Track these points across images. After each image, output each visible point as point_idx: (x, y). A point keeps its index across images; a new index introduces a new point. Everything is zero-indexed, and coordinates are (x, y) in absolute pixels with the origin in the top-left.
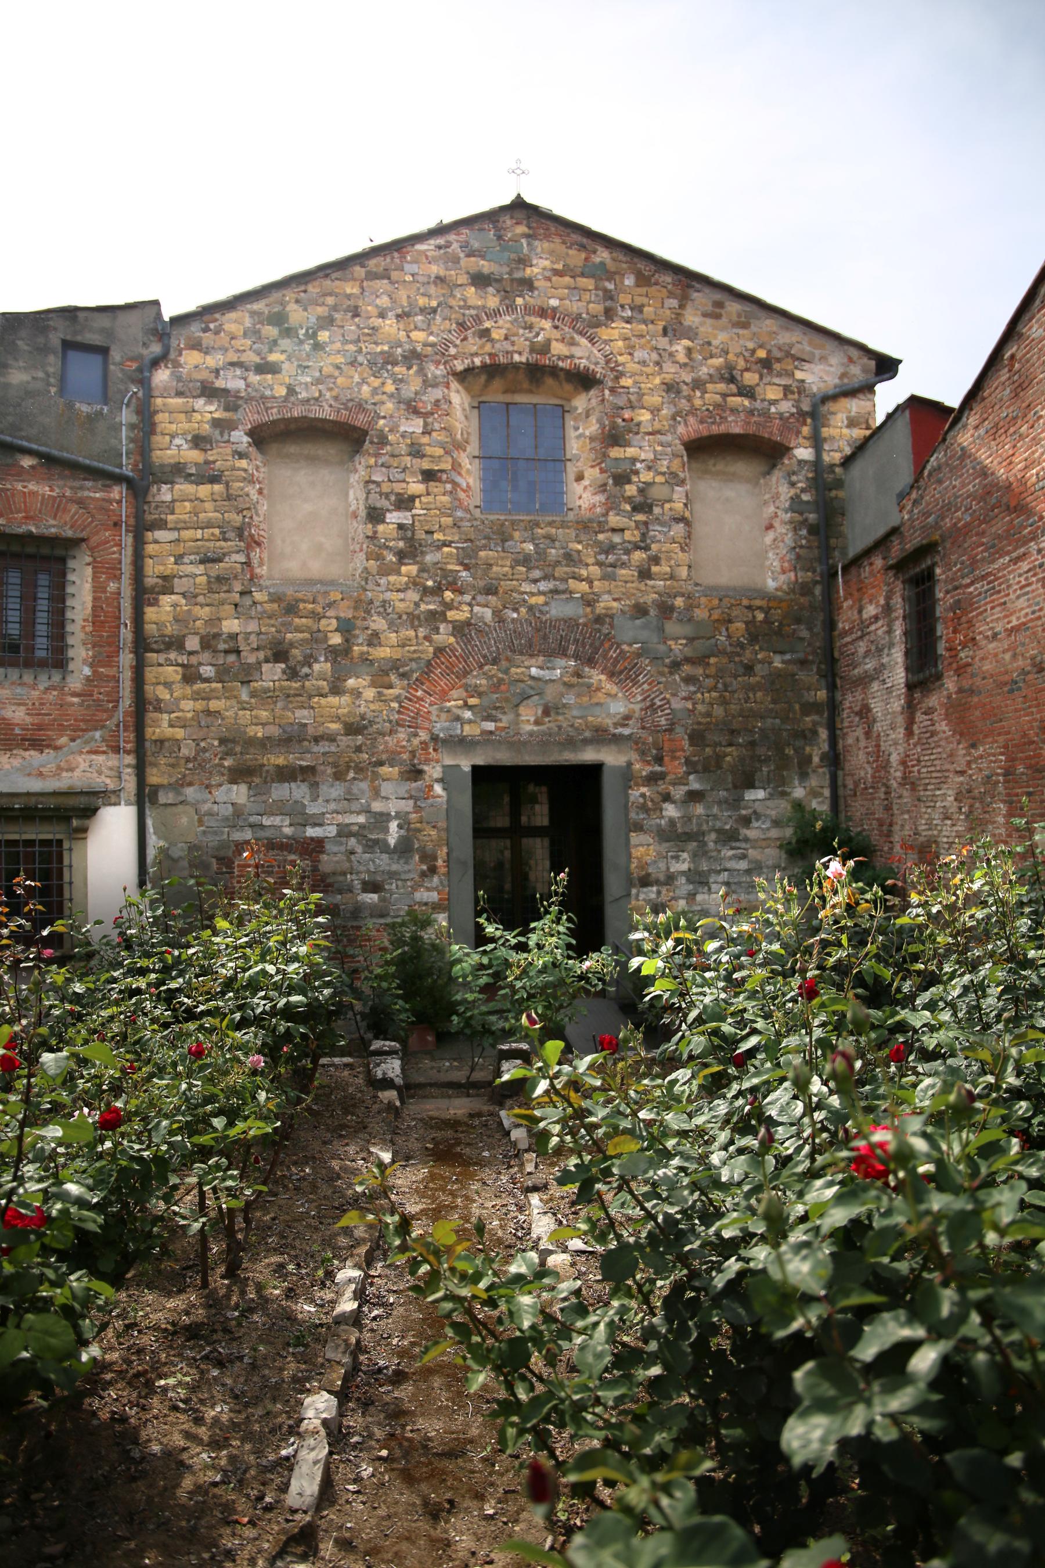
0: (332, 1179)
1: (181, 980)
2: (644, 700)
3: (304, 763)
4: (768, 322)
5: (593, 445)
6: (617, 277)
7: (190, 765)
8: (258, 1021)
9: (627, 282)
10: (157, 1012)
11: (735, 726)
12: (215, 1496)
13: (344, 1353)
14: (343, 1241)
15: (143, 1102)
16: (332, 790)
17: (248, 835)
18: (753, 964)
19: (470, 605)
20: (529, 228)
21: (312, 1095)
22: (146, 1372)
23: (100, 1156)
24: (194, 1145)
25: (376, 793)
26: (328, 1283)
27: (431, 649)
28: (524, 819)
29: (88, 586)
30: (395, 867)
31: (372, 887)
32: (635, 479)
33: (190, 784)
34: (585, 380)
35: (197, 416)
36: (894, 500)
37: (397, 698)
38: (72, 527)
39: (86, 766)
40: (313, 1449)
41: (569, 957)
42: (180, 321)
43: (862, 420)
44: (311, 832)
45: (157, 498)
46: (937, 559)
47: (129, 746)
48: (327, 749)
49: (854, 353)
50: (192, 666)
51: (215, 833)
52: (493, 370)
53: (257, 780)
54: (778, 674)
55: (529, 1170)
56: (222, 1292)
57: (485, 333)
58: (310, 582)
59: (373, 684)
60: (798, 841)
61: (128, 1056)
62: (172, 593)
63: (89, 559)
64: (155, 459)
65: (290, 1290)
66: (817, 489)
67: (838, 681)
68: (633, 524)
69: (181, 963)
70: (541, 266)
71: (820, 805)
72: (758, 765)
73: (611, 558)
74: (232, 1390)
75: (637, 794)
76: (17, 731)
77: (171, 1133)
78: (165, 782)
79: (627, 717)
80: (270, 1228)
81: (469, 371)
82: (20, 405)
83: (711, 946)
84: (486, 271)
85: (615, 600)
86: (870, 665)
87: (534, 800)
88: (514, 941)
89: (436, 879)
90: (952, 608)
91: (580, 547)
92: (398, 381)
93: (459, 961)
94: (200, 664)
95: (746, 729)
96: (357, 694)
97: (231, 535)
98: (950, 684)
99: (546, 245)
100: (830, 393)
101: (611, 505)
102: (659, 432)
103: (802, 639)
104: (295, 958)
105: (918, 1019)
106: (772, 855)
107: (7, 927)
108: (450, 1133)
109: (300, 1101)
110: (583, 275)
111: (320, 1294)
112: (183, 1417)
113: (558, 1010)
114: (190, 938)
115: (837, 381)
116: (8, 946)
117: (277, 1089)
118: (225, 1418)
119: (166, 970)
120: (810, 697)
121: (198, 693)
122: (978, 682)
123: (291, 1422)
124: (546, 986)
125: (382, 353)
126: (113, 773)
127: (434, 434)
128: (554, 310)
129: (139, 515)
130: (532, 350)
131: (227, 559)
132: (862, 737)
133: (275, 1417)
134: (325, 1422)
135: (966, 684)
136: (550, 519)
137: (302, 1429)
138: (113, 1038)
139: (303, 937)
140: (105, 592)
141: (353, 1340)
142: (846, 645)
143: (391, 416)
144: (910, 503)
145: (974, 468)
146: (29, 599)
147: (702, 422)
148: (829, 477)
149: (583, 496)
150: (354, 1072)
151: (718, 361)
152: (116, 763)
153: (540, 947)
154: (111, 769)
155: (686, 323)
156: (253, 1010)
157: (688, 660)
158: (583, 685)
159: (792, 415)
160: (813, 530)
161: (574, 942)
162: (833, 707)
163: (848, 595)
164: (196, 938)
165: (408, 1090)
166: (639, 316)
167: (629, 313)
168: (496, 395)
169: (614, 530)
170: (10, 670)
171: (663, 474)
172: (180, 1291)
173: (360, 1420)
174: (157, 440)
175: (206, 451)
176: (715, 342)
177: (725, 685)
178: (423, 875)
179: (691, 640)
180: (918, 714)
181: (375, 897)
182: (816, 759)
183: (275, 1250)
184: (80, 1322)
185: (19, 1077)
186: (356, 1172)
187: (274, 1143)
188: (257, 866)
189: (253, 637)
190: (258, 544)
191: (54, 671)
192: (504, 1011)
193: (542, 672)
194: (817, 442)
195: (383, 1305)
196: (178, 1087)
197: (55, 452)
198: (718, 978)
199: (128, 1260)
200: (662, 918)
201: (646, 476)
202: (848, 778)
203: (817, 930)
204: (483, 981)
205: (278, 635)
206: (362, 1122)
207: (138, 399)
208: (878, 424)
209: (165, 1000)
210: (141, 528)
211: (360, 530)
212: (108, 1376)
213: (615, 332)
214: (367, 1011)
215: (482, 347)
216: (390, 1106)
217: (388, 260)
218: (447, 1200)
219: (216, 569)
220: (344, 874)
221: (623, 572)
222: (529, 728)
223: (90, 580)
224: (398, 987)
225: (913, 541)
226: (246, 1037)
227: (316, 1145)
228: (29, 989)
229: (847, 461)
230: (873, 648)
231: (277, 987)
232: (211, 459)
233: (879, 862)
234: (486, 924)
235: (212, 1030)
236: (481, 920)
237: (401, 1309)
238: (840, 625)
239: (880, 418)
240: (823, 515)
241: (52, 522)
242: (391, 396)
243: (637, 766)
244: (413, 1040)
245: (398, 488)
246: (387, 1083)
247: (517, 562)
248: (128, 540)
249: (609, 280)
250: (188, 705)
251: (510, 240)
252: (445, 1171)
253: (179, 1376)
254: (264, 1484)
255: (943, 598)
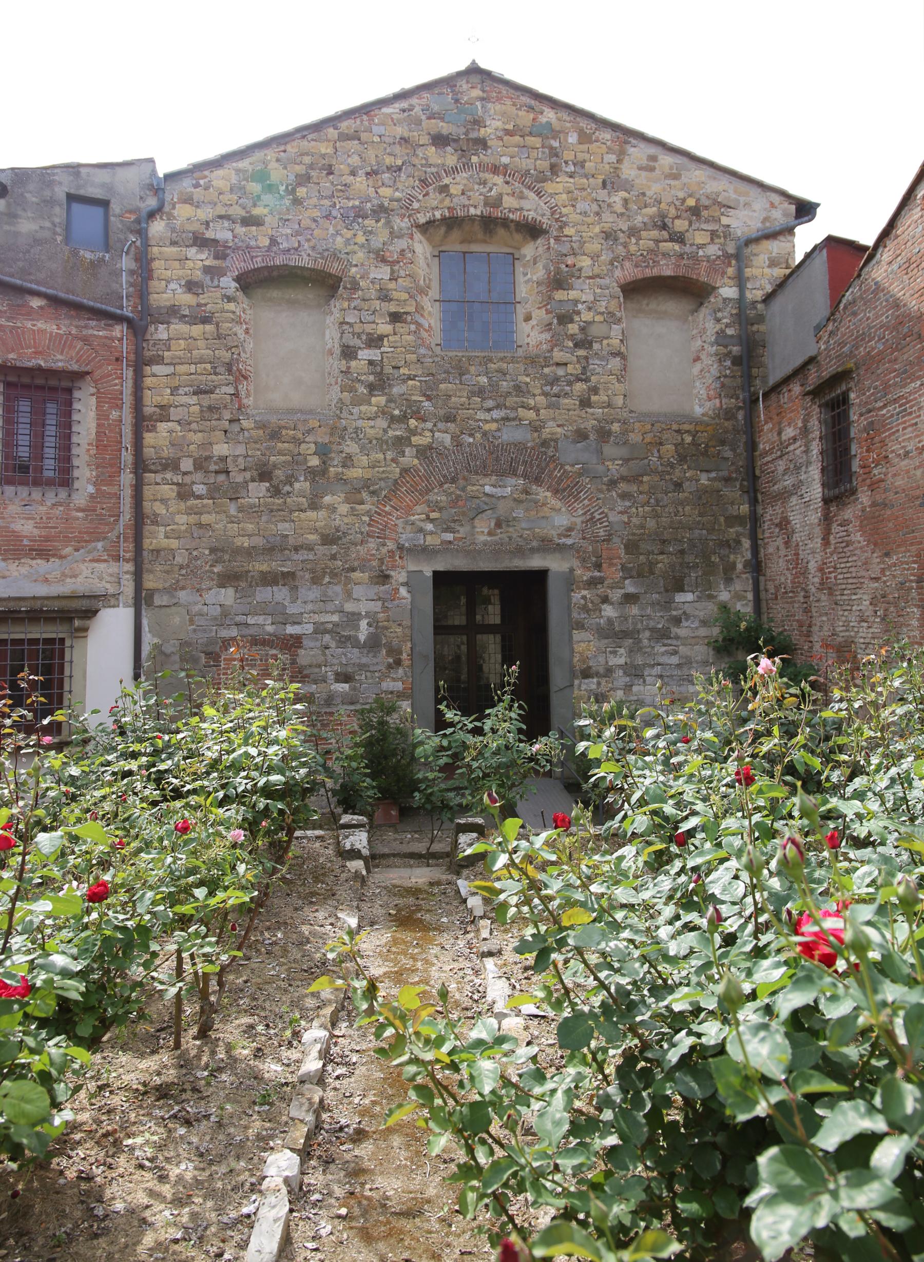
0: (301, 944)
1: (170, 762)
2: (585, 514)
3: (286, 570)
4: (697, 173)
5: (540, 288)
6: (562, 136)
7: (184, 572)
8: (240, 798)
9: (570, 140)
10: (147, 792)
11: (666, 536)
12: (174, 1253)
13: (308, 1111)
14: (310, 1003)
15: (129, 875)
16: (310, 593)
17: (234, 632)
18: (689, 750)
19: (431, 431)
20: (483, 91)
21: (287, 866)
22: (115, 1131)
23: (86, 927)
24: (175, 914)
25: (349, 595)
26: (295, 1043)
27: (398, 470)
28: (478, 617)
29: (92, 414)
30: (364, 660)
31: (345, 677)
32: (577, 318)
33: (183, 588)
34: (533, 231)
35: (190, 264)
36: (812, 333)
37: (368, 513)
38: (77, 361)
39: (87, 573)
40: (274, 1207)
41: (520, 741)
42: (169, 177)
43: (782, 260)
44: (291, 630)
45: (155, 337)
46: (852, 384)
47: (128, 555)
48: (306, 557)
49: (776, 198)
50: (186, 485)
51: (205, 631)
52: (452, 223)
53: (243, 584)
54: (705, 491)
55: (484, 936)
56: (193, 1053)
57: (444, 189)
58: (291, 411)
59: (347, 501)
60: (724, 640)
61: (117, 833)
62: (169, 421)
63: (93, 390)
64: (152, 302)
65: (259, 1049)
66: (740, 324)
67: (760, 497)
68: (575, 359)
69: (170, 747)
70: (494, 126)
71: (745, 608)
72: (686, 571)
73: (556, 389)
74: (197, 1148)
75: (579, 596)
76: (26, 542)
77: (154, 903)
78: (161, 586)
79: (570, 529)
80: (242, 990)
81: (430, 223)
82: (28, 251)
83: (649, 733)
84: (445, 132)
85: (558, 426)
86: (789, 482)
87: (487, 601)
88: (470, 726)
89: (401, 671)
90: (865, 430)
91: (528, 380)
92: (368, 233)
93: (421, 743)
94: (194, 483)
95: (676, 540)
96: (332, 509)
97: (221, 369)
98: (864, 498)
99: (498, 107)
100: (754, 236)
101: (555, 343)
102: (598, 276)
103: (727, 459)
104: (275, 742)
105: (850, 808)
106: (701, 651)
107: (9, 717)
108: (411, 900)
109: (275, 871)
110: (531, 134)
111: (285, 1053)
112: (148, 1175)
113: (510, 788)
114: (180, 724)
115: (760, 225)
116: (10, 735)
117: (255, 859)
118: (188, 1176)
119: (156, 753)
120: (733, 510)
121: (191, 509)
122: (891, 496)
123: (253, 1180)
124: (499, 766)
125: (353, 207)
126: (113, 579)
127: (400, 280)
128: (506, 166)
129: (138, 352)
130: (486, 204)
131: (217, 391)
132: (782, 547)
133: (238, 1175)
134: (287, 1181)
135: (879, 498)
136: (502, 355)
137: (263, 1187)
138: (104, 816)
139: (282, 723)
140: (108, 419)
141: (316, 1099)
142: (766, 464)
143: (362, 265)
144: (827, 334)
145: (887, 301)
146: (38, 424)
147: (636, 266)
148: (752, 313)
149: (531, 334)
150: (325, 844)
151: (652, 211)
152: (116, 570)
153: (494, 731)
154: (111, 575)
155: (623, 177)
156: (235, 788)
157: (623, 478)
158: (531, 501)
159: (719, 257)
160: (737, 361)
161: (524, 727)
162: (755, 520)
163: (769, 419)
164: (186, 724)
165: (373, 860)
166: (581, 171)
167: (572, 169)
168: (454, 245)
169: (558, 364)
170: (20, 488)
171: (602, 314)
172: (153, 1052)
173: (321, 1178)
174: (154, 284)
175: (198, 295)
176: (648, 193)
177: (657, 501)
178: (390, 667)
179: (626, 460)
180: (834, 525)
181: (346, 686)
182: (740, 566)
183: (246, 1011)
184: (55, 1086)
185: (13, 855)
186: (323, 937)
187: (250, 910)
188: (242, 660)
189: (240, 460)
190: (246, 378)
191: (60, 489)
192: (462, 788)
193: (494, 490)
194: (741, 281)
195: (347, 1064)
196: (163, 861)
197: (62, 295)
198: (656, 762)
199: (105, 1024)
200: (606, 707)
201: (587, 316)
202: (769, 583)
203: (745, 721)
204: (442, 762)
205: (263, 458)
206: (331, 890)
207: (136, 247)
208: (797, 262)
209: (155, 780)
210: (140, 364)
211: (335, 366)
212: (77, 1136)
213: (559, 186)
214: (338, 787)
215: (442, 201)
216: (357, 875)
217: (358, 122)
218: (409, 963)
219: (206, 400)
220: (320, 666)
221: (566, 401)
222: (483, 538)
223: (94, 408)
224: (367, 767)
225: (829, 369)
226: (228, 813)
227: (288, 912)
228: (28, 774)
229: (768, 298)
230: (792, 466)
231: (257, 768)
232: (203, 302)
233: (800, 660)
234: (446, 710)
235: (198, 807)
236: (442, 707)
237: (364, 1068)
238: (761, 446)
239: (799, 257)
240: (745, 352)
241: (59, 357)
242: (362, 246)
243: (578, 572)
244: (379, 814)
245: (369, 328)
246: (354, 854)
247: (473, 394)
248: (129, 374)
249: (554, 138)
250: (182, 519)
251: (466, 103)
252: (407, 936)
253: (147, 1135)
254: (223, 1241)
255: (857, 420)
